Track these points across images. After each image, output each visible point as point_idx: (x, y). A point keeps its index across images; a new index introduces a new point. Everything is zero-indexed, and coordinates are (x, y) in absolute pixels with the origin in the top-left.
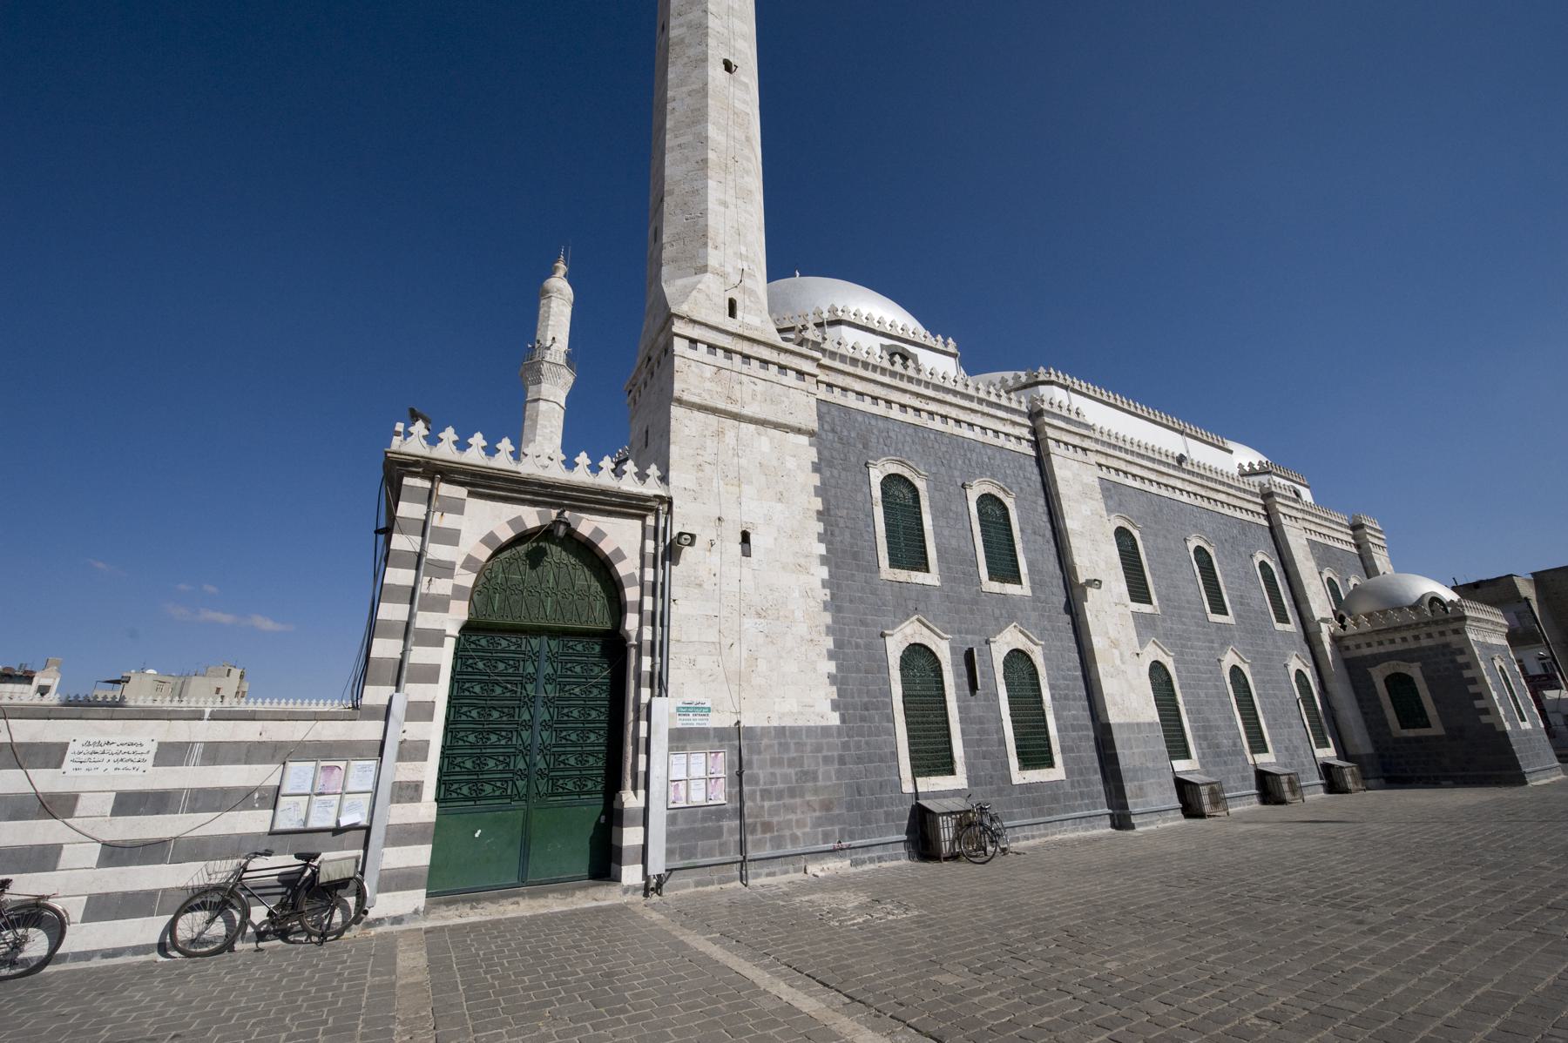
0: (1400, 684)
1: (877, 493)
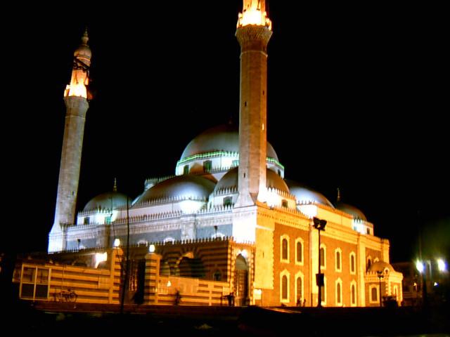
0: (374, 290)
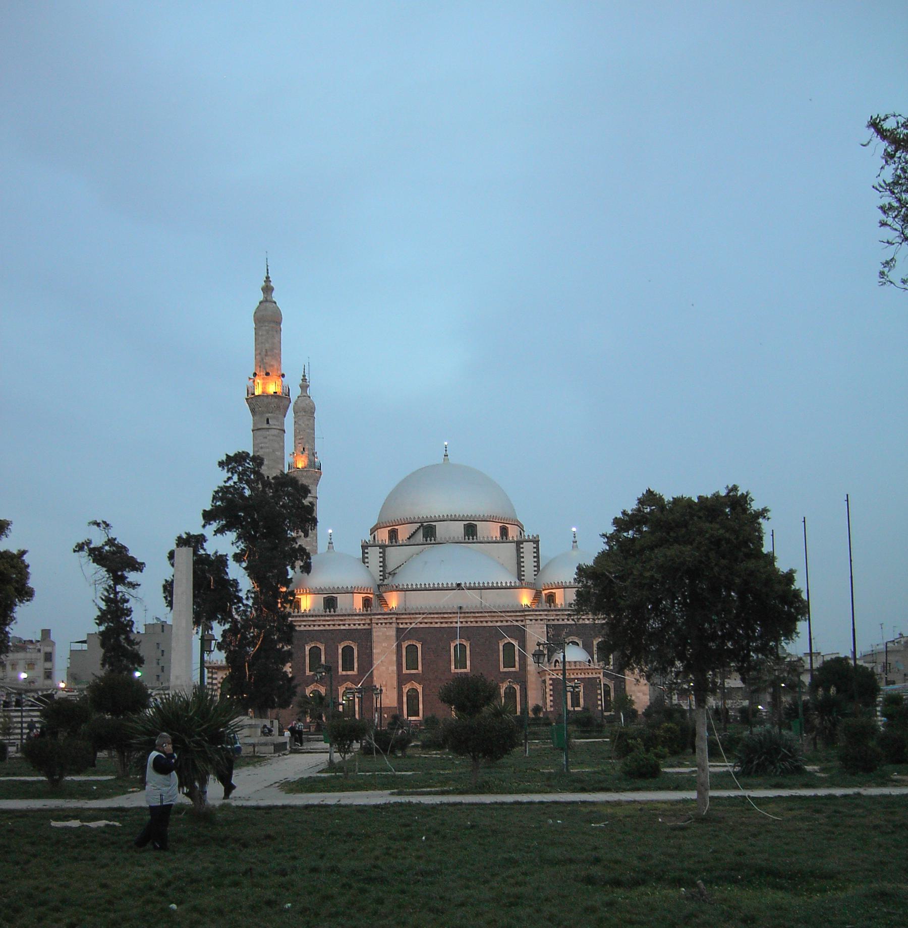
1: (340, 651)
